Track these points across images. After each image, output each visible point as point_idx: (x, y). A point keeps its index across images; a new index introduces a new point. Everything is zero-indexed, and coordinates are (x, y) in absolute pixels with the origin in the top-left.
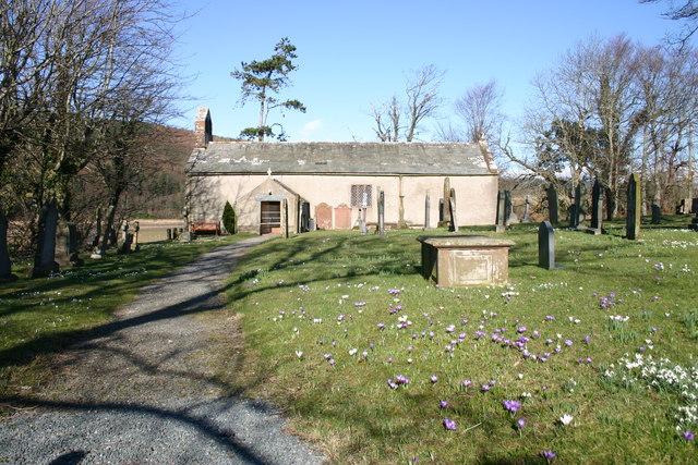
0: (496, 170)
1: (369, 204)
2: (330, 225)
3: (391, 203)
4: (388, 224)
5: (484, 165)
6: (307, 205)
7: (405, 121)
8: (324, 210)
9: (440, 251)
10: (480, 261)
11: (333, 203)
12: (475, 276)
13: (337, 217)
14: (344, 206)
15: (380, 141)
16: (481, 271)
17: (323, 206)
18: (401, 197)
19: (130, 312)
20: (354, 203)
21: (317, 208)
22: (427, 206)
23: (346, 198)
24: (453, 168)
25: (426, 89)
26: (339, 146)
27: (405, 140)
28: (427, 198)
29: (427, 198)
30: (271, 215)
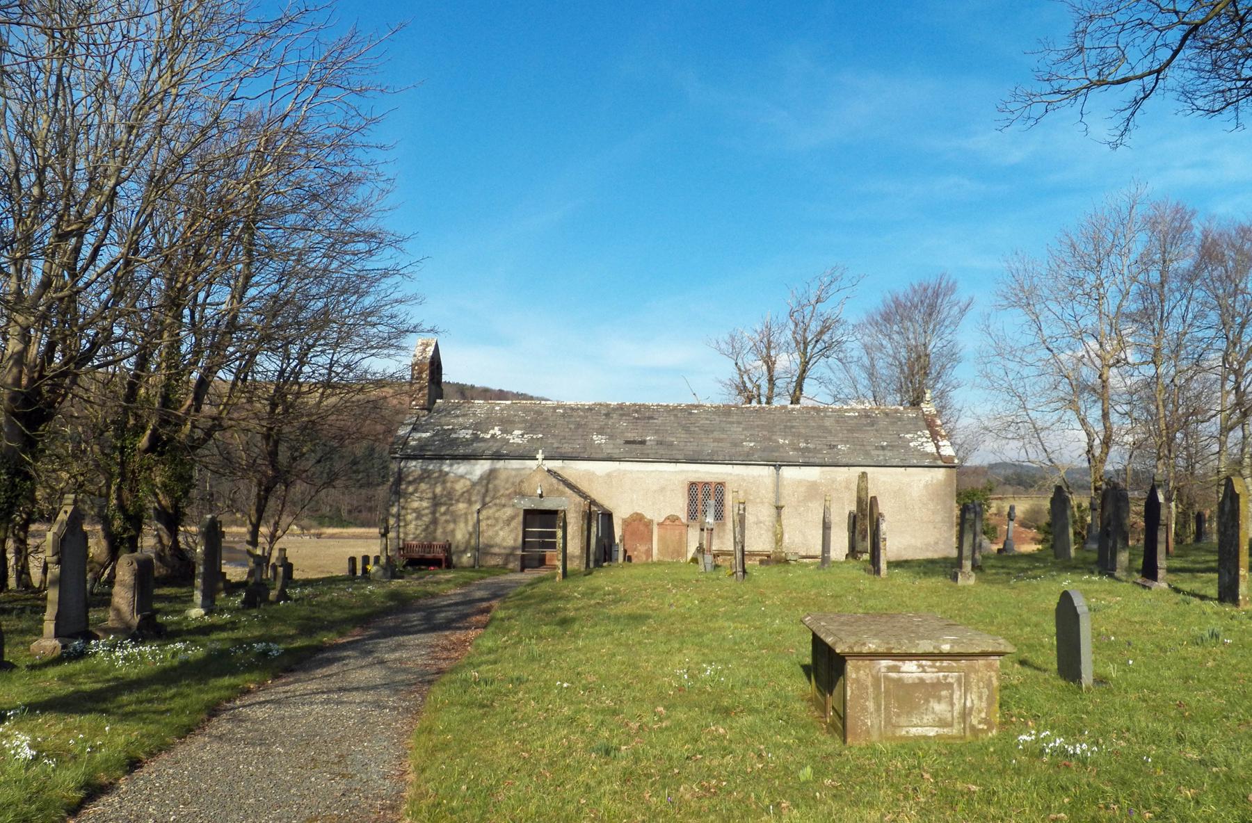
0: (951, 458)
1: (719, 516)
2: (649, 553)
3: (759, 515)
4: (752, 554)
5: (930, 448)
6: (608, 516)
7: (786, 362)
8: (639, 524)
9: (850, 666)
10: (937, 686)
11: (655, 514)
12: (928, 718)
13: (661, 539)
14: (673, 519)
15: (740, 400)
16: (940, 708)
17: (638, 518)
18: (779, 508)
19: (594, 525)
20: (692, 515)
21: (626, 523)
22: (826, 527)
23: (679, 506)
24: (874, 453)
25: (825, 309)
26: (669, 410)
27: (786, 401)
28: (826, 511)
29: (826, 511)
30: (541, 535)
